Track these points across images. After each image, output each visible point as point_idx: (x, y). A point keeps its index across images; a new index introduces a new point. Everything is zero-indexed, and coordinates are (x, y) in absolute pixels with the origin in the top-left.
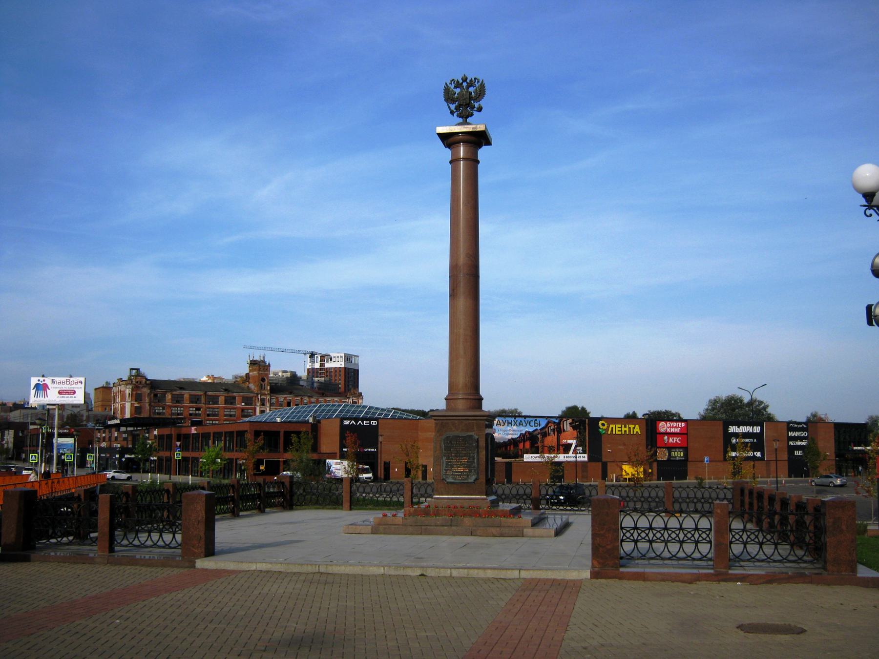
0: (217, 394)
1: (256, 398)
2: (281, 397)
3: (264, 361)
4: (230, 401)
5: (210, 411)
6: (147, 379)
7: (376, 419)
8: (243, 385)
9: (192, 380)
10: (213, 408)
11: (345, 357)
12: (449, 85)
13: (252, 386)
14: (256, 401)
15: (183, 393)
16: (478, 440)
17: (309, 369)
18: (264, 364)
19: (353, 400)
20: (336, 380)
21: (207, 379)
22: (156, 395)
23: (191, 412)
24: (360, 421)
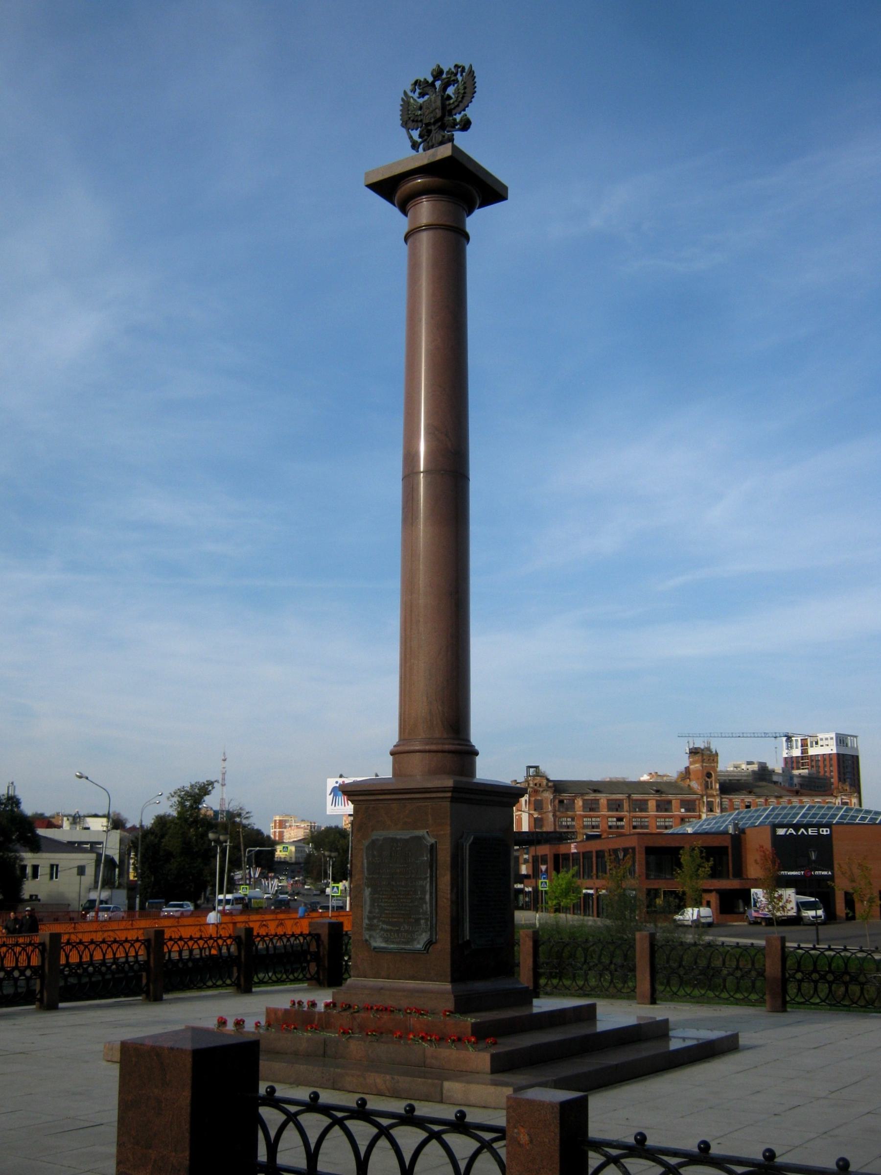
0: (646, 797)
1: (701, 801)
2: (736, 798)
3: (708, 749)
4: (664, 806)
5: (636, 821)
6: (548, 780)
7: (828, 825)
8: (682, 784)
9: (621, 780)
10: (641, 818)
11: (837, 738)
12: (411, 94)
13: (695, 785)
14: (701, 805)
15: (598, 798)
16: (433, 848)
17: (786, 758)
18: (708, 752)
19: (842, 799)
20: (825, 772)
21: (649, 777)
22: (561, 802)
23: (610, 824)
24: (802, 830)
